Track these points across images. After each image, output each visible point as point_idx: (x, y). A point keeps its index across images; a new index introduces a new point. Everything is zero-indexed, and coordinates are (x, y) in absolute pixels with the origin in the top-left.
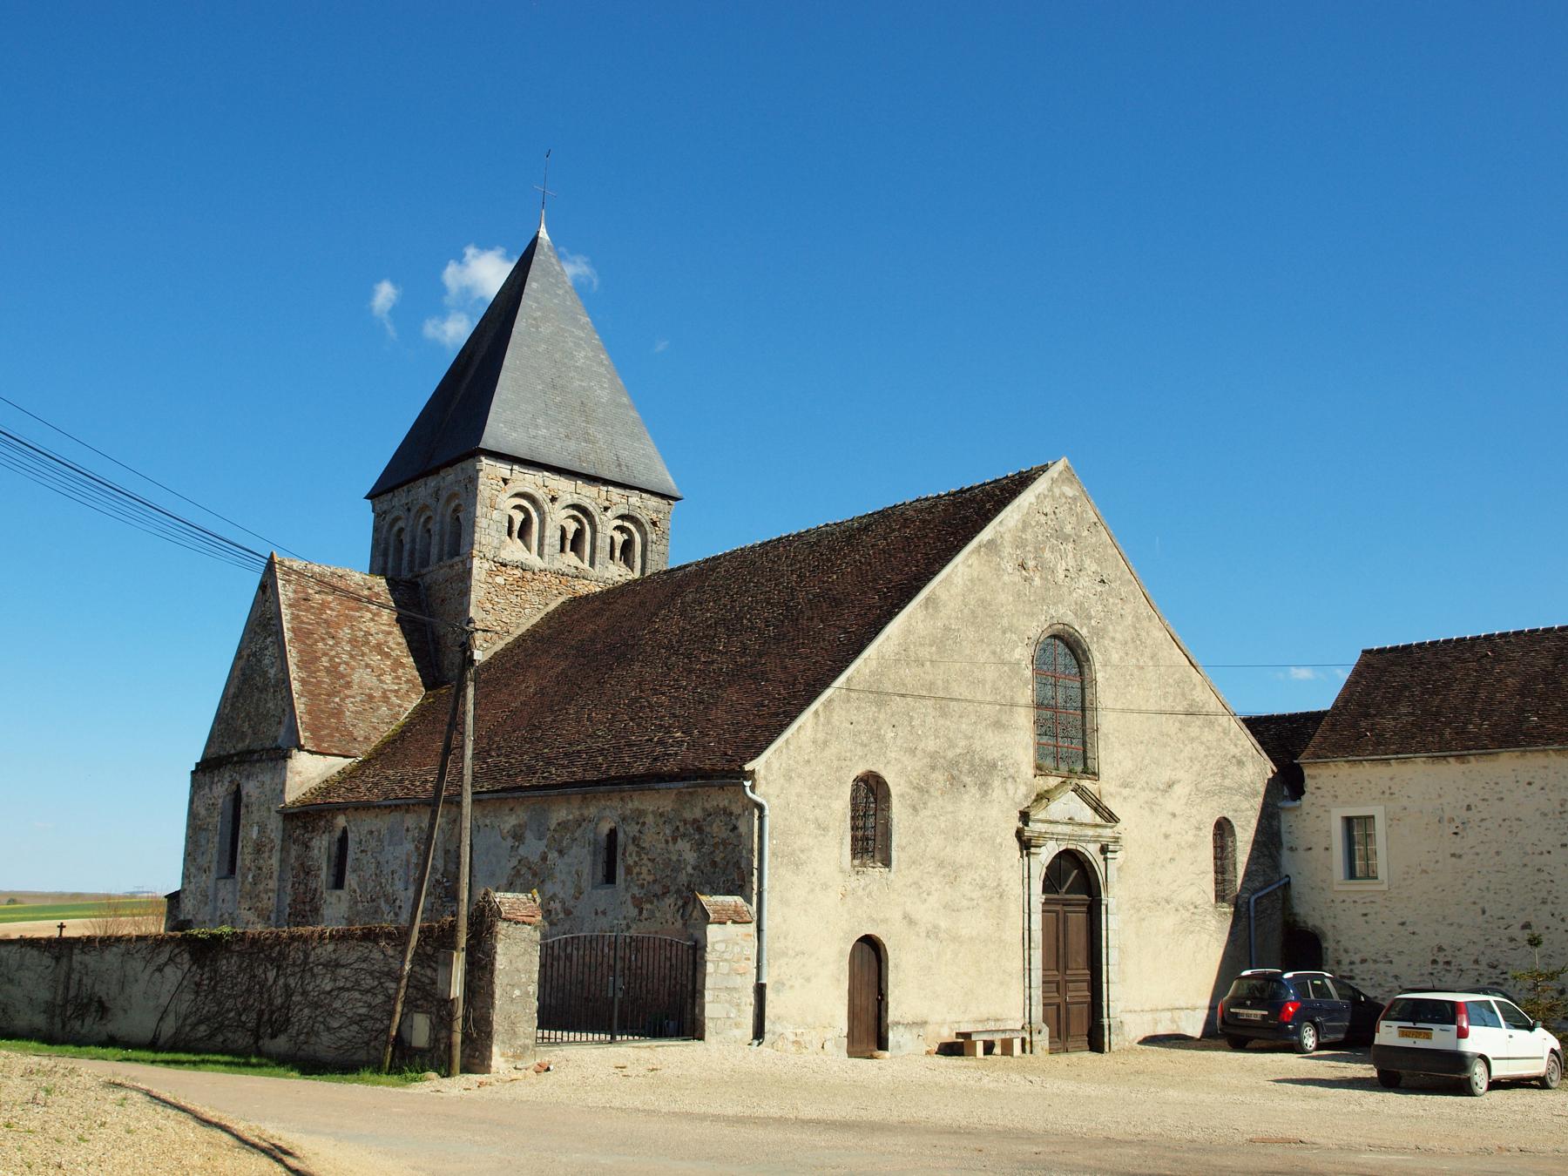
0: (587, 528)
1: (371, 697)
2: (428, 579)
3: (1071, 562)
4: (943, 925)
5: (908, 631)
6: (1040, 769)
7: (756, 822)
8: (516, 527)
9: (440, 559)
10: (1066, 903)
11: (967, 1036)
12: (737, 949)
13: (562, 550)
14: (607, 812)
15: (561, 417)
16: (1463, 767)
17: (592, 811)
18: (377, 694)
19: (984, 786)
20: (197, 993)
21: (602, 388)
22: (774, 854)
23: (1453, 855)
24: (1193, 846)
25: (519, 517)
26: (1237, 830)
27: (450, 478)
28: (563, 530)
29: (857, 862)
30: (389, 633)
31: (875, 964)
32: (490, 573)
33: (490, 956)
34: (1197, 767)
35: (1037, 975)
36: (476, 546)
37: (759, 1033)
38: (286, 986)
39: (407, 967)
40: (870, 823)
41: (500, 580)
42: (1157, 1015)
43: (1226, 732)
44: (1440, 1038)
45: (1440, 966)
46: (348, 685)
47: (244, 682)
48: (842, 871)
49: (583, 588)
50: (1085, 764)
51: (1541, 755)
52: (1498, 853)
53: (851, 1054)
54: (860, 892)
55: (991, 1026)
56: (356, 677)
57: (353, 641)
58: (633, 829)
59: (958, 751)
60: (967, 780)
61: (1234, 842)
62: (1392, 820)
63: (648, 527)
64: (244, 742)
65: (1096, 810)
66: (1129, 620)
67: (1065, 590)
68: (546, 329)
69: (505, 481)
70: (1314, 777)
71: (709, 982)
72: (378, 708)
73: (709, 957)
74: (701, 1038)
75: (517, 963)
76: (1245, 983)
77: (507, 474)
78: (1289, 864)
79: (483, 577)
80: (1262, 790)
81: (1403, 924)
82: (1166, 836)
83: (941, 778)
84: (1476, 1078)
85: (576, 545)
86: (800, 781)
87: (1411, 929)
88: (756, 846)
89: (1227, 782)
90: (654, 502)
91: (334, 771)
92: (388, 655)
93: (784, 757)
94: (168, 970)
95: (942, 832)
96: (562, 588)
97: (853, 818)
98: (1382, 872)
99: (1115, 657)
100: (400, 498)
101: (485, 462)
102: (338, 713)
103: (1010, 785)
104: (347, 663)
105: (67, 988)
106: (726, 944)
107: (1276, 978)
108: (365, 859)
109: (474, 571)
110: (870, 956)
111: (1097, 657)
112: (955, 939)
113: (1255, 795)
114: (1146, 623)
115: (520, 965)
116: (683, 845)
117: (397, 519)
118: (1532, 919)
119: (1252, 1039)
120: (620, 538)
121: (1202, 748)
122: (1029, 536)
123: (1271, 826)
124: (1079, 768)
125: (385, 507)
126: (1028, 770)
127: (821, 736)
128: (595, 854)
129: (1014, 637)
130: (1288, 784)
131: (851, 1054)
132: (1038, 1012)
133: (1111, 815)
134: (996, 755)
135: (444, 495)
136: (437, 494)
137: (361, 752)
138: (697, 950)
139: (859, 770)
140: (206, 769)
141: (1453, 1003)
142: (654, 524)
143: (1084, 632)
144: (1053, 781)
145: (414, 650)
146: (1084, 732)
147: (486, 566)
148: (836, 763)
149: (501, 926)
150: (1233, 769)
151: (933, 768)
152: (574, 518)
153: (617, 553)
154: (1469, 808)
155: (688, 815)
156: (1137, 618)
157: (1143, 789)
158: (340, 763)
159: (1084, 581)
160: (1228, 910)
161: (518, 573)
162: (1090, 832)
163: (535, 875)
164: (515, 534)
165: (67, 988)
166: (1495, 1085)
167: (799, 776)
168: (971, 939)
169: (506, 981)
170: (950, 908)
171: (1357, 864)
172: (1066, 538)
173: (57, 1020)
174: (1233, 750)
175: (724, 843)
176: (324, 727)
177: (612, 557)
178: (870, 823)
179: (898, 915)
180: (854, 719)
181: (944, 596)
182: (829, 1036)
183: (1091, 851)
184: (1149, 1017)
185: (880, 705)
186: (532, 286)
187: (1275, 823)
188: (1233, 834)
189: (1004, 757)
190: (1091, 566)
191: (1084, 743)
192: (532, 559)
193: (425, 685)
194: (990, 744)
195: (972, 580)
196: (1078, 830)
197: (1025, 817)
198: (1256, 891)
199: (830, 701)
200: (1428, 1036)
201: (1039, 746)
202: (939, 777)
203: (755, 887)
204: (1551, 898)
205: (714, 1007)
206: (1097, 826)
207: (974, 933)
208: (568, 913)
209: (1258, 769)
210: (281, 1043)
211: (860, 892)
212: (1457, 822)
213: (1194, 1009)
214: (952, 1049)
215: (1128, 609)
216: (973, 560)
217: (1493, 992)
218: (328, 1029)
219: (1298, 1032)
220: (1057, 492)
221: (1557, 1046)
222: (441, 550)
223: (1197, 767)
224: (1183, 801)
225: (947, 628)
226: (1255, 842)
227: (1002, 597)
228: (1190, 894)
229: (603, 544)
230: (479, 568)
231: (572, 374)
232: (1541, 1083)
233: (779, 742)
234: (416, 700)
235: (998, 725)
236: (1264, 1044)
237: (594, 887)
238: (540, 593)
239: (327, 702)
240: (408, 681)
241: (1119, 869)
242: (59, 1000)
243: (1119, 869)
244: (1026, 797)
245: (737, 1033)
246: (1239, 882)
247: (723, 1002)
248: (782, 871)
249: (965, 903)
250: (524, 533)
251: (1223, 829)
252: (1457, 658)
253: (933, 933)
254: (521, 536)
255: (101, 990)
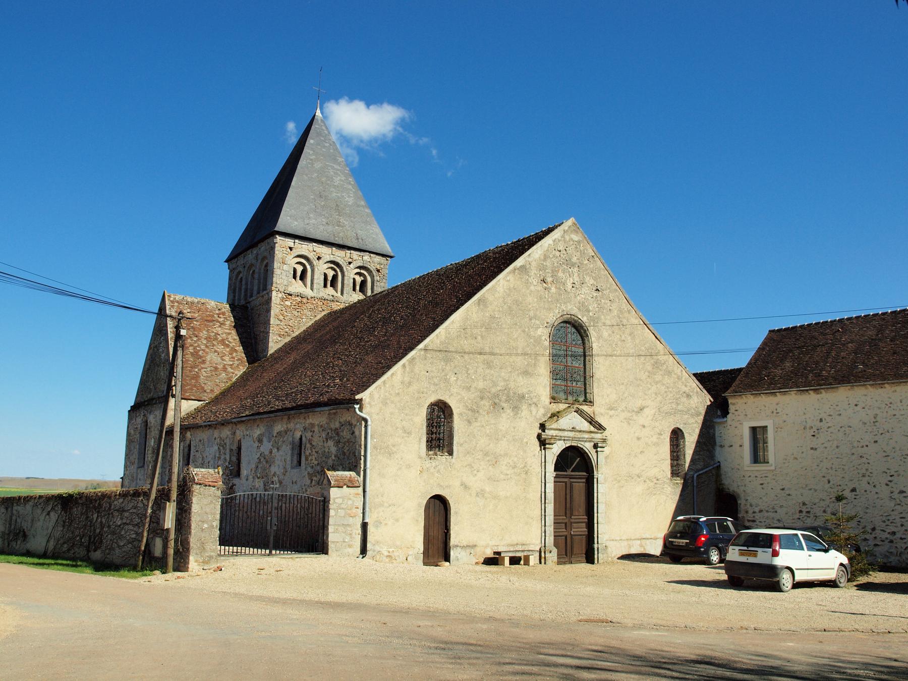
0: (339, 274)
1: (216, 368)
2: (252, 304)
3: (576, 279)
4: (487, 489)
5: (466, 319)
6: (554, 399)
7: (363, 429)
8: (299, 274)
9: (258, 293)
10: (571, 477)
11: (499, 553)
12: (350, 502)
13: (325, 286)
14: (298, 426)
15: (324, 213)
16: (819, 396)
17: (291, 426)
18: (220, 367)
19: (516, 409)
20: (64, 526)
21: (349, 197)
22: (375, 447)
23: (812, 449)
24: (656, 444)
25: (300, 269)
26: (686, 435)
27: (263, 248)
28: (326, 275)
29: (431, 453)
30: (229, 334)
31: (443, 512)
32: (282, 299)
33: (189, 503)
34: (659, 398)
35: (550, 519)
36: (274, 285)
37: (364, 551)
38: (101, 522)
39: (150, 511)
40: (439, 430)
41: (288, 303)
42: (630, 542)
43: (679, 378)
44: (762, 556)
45: (804, 514)
46: (204, 362)
47: (152, 362)
48: (420, 458)
49: (336, 307)
50: (585, 396)
51: (863, 388)
52: (837, 447)
53: (425, 564)
54: (432, 470)
55: (520, 548)
56: (208, 358)
57: (208, 338)
58: (309, 434)
59: (499, 388)
60: (505, 405)
61: (684, 442)
62: (777, 429)
63: (375, 273)
64: (151, 396)
65: (590, 423)
66: (615, 313)
67: (572, 295)
68: (318, 165)
69: (291, 249)
70: (734, 404)
71: (331, 521)
72: (220, 374)
73: (331, 506)
74: (327, 553)
75: (206, 508)
76: (681, 524)
77: (292, 245)
78: (721, 455)
79: (278, 301)
80: (703, 412)
81: (783, 489)
82: (638, 439)
83: (487, 404)
84: (784, 581)
85: (333, 284)
86: (393, 406)
87: (788, 492)
88: (363, 443)
89: (680, 407)
90: (378, 259)
91: (193, 409)
92: (228, 346)
93: (382, 391)
94: (52, 514)
95: (488, 435)
96: (324, 307)
97: (428, 426)
98: (771, 457)
99: (605, 334)
100: (241, 261)
101: (279, 239)
102: (196, 377)
103: (533, 408)
104: (204, 350)
105: (10, 524)
106: (342, 502)
107: (696, 522)
108: (198, 455)
109: (273, 298)
110: (439, 509)
111: (593, 333)
112: (496, 497)
113: (698, 415)
114: (626, 315)
115: (208, 510)
116: (331, 443)
117: (240, 272)
118: (856, 485)
119: (684, 557)
120: (359, 279)
121: (663, 388)
122: (548, 263)
123: (708, 432)
124: (581, 399)
125: (234, 266)
126: (545, 398)
127: (407, 379)
128: (293, 449)
129: (538, 322)
130: (718, 409)
131: (425, 564)
132: (550, 540)
133: (600, 425)
134: (525, 391)
135: (260, 257)
136: (256, 258)
137: (207, 397)
138: (325, 503)
139: (433, 399)
140: (134, 410)
141: (771, 535)
142: (378, 271)
143: (585, 319)
144: (562, 406)
145: (243, 343)
146: (585, 378)
147: (280, 295)
148: (416, 395)
149: (196, 488)
150: (684, 399)
151: (482, 398)
152: (332, 268)
153: (358, 288)
154: (821, 420)
155: (333, 426)
156: (621, 311)
157: (623, 411)
158: (197, 404)
159: (585, 290)
160: (679, 481)
161: (299, 299)
162: (586, 436)
163: (267, 462)
164: (298, 278)
165: (10, 524)
166: (797, 585)
167: (392, 402)
168: (506, 497)
169: (198, 519)
170: (491, 479)
171: (757, 456)
172: (573, 265)
173: (6, 542)
174: (684, 389)
175: (348, 441)
176: (188, 385)
177: (354, 289)
178: (439, 430)
179: (458, 483)
180: (429, 369)
181: (491, 298)
182: (410, 553)
183: (588, 447)
184: (626, 543)
185: (447, 360)
186: (310, 141)
187: (712, 431)
188: (683, 437)
189: (530, 392)
190: (590, 281)
191: (585, 384)
192: (307, 292)
193: (248, 361)
194: (521, 384)
195: (509, 289)
196: (578, 435)
197: (543, 427)
198: (698, 470)
199: (413, 359)
200: (755, 556)
201: (554, 387)
202: (486, 404)
203: (362, 466)
204: (868, 473)
205: (334, 536)
206: (591, 432)
207: (508, 495)
208: (281, 483)
209: (702, 400)
210: (97, 555)
211: (432, 470)
212: (815, 429)
213: (656, 539)
214: (493, 561)
215: (614, 306)
216: (510, 277)
217: (799, 529)
218: (119, 546)
219: (707, 552)
220: (567, 238)
221: (845, 561)
222: (259, 288)
223: (659, 398)
224: (650, 418)
225: (492, 317)
226: (698, 442)
227: (530, 299)
228: (655, 472)
229: (349, 283)
230: (276, 297)
231: (332, 189)
232: (831, 584)
233: (379, 382)
234: (242, 370)
235: (526, 373)
236: (689, 559)
237: (292, 468)
238: (311, 310)
239: (190, 371)
240: (239, 360)
241: (606, 458)
242: (7, 532)
243: (606, 458)
244: (544, 415)
245: (350, 550)
246: (687, 465)
247: (341, 530)
248: (380, 457)
249: (502, 476)
250: (303, 277)
251: (677, 435)
252: (822, 333)
253: (481, 494)
254: (331, 286)
255: (25, 526)
